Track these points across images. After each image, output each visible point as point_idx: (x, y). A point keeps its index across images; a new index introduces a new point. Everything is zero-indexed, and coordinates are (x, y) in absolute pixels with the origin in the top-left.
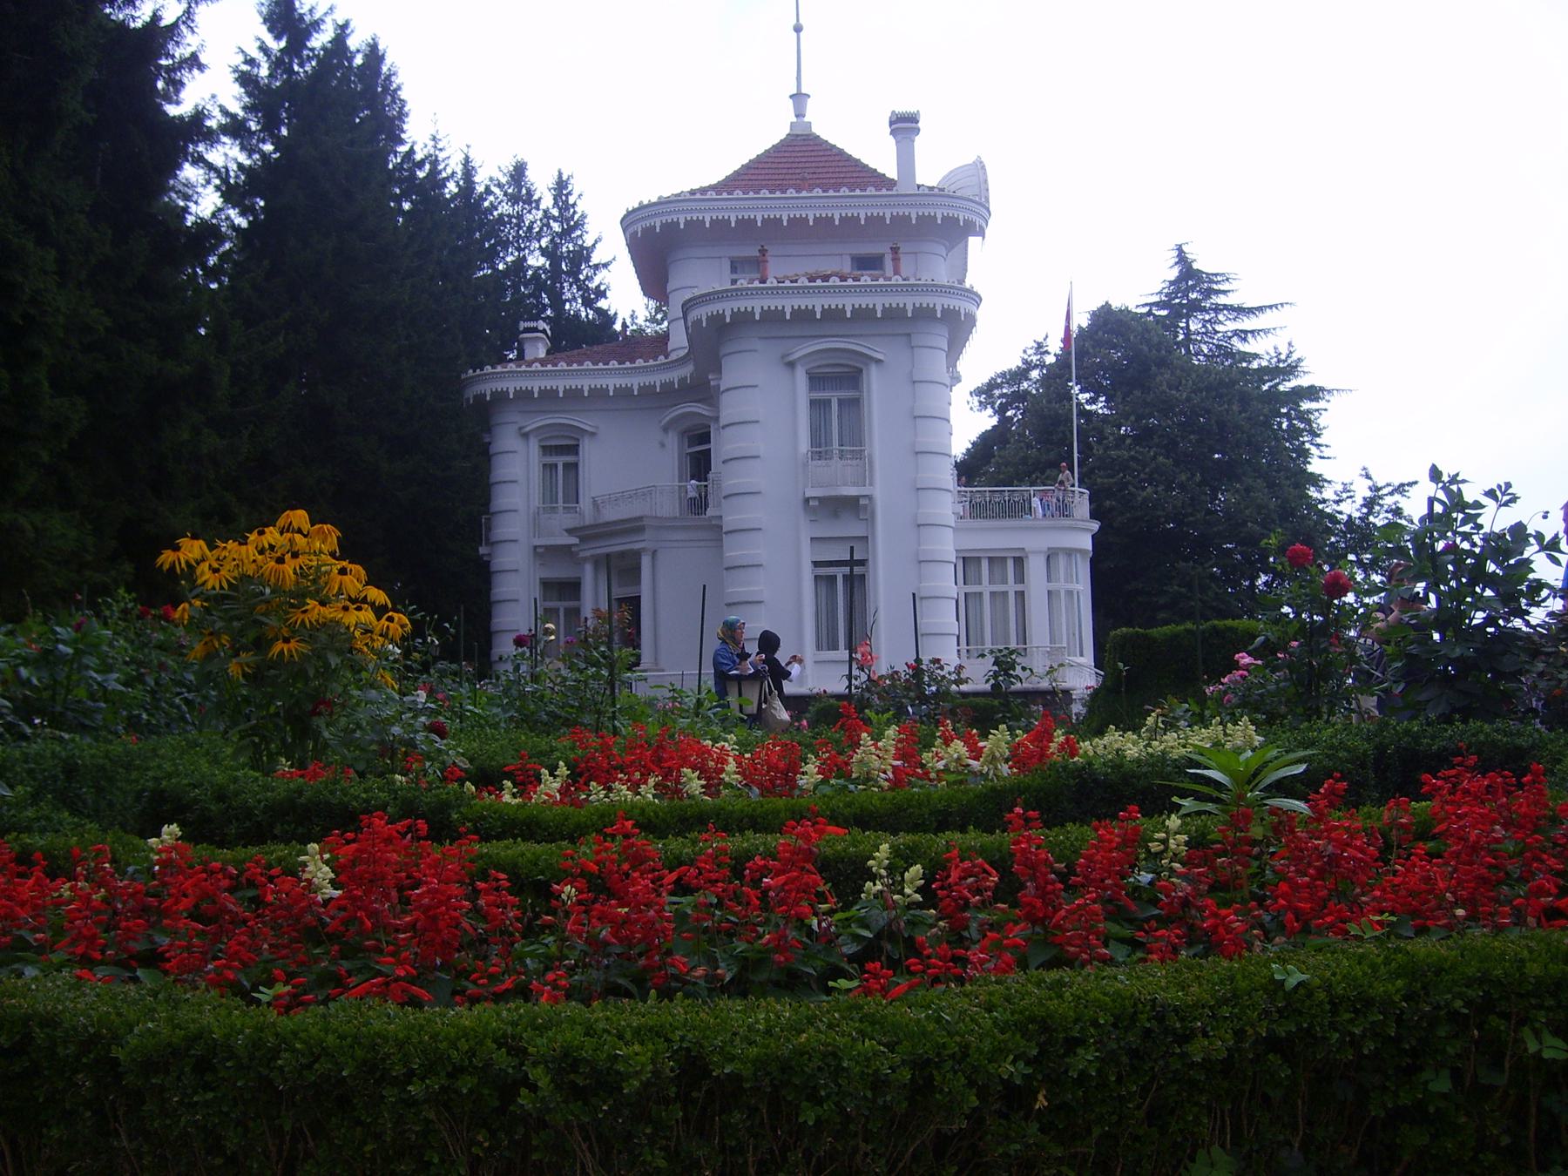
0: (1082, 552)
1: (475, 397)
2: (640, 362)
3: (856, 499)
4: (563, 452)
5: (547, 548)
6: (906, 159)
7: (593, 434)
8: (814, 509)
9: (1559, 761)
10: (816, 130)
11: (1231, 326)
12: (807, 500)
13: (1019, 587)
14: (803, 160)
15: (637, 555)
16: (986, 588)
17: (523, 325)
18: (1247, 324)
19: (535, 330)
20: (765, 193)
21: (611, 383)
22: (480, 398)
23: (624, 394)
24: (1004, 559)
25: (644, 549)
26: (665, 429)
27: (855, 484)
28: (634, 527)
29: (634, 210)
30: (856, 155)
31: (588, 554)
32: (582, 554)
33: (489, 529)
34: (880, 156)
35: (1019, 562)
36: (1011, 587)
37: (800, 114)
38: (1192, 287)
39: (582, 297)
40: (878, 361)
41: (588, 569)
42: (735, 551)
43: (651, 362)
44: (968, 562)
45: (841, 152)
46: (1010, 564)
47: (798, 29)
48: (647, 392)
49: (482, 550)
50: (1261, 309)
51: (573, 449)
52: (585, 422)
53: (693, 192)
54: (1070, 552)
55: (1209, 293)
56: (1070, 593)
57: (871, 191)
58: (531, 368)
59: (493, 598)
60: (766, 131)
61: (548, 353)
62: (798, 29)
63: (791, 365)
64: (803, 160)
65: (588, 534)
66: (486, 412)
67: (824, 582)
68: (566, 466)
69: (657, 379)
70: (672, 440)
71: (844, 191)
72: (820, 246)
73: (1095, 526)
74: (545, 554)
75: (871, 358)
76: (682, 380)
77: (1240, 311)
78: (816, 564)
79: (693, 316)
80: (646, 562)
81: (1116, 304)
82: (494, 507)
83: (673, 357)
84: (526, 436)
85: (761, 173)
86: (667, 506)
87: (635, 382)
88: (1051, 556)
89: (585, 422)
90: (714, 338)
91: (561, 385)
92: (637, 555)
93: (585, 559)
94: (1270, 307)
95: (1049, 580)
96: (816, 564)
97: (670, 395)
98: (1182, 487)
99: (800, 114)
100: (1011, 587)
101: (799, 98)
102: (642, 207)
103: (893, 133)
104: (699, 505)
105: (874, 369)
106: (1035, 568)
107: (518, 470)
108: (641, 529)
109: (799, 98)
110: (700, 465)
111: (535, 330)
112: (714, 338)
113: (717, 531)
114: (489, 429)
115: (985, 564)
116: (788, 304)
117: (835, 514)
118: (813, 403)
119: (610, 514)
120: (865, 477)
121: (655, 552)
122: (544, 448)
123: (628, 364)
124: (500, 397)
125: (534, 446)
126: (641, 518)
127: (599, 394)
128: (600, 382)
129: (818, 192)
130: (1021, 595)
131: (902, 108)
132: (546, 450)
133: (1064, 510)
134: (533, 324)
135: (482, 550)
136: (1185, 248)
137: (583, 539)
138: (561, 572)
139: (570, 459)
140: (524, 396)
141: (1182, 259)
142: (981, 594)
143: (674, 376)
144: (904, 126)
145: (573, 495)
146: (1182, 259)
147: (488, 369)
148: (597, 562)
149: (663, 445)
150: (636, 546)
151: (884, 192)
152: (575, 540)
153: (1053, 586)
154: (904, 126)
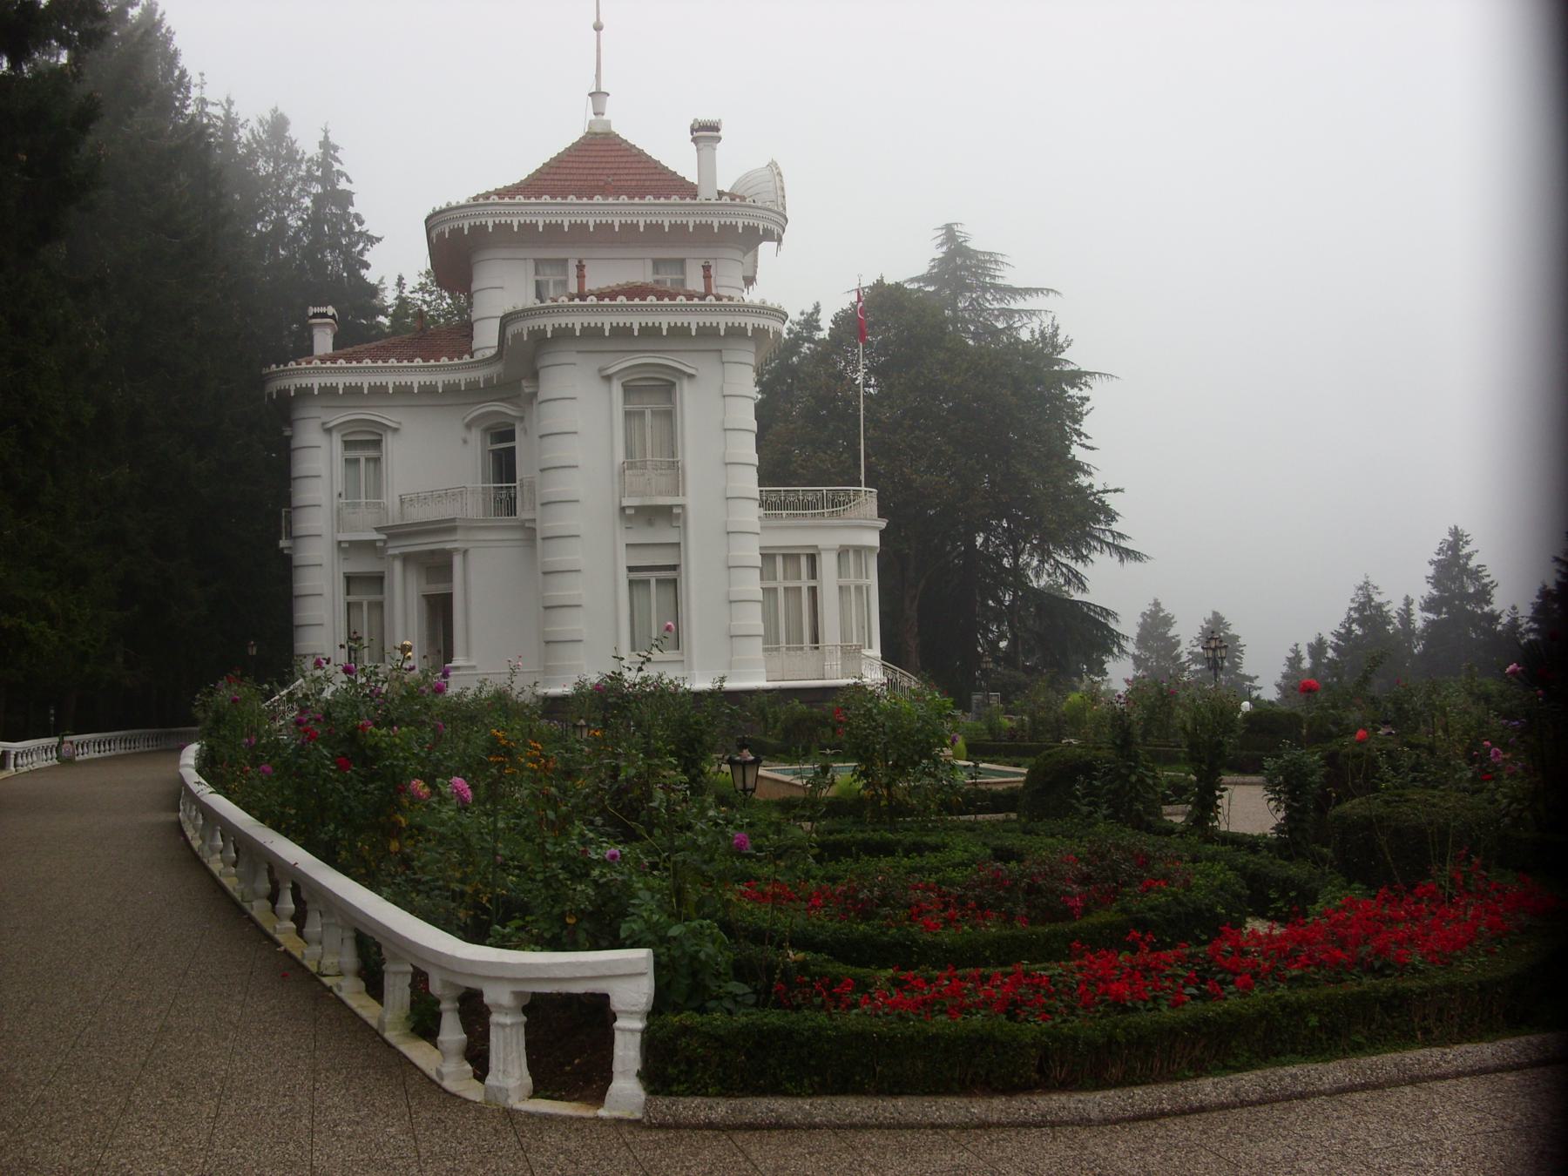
0: (870, 548)
1: (279, 392)
2: (444, 360)
3: (671, 507)
4: (365, 444)
5: (350, 542)
6: (706, 166)
7: (396, 430)
10: (615, 129)
12: (623, 509)
13: (812, 583)
15: (448, 555)
16: (780, 584)
17: (312, 311)
19: (324, 315)
20: (572, 199)
21: (416, 380)
22: (283, 394)
23: (428, 391)
24: (798, 556)
25: (456, 549)
26: (468, 426)
27: (668, 493)
28: (446, 527)
29: (442, 212)
31: (396, 552)
32: (391, 552)
33: (290, 523)
34: (680, 159)
35: (812, 559)
36: (805, 583)
38: (961, 266)
39: (344, 261)
40: (691, 376)
41: (398, 566)
42: (560, 556)
43: (456, 361)
44: (768, 556)
45: (641, 153)
46: (804, 561)
47: (598, 28)
48: (452, 390)
49: (283, 543)
51: (377, 444)
52: (388, 416)
53: (500, 193)
54: (859, 550)
56: (859, 588)
57: (675, 199)
59: (296, 593)
61: (337, 345)
62: (598, 28)
64: (600, 163)
65: (395, 533)
66: (285, 409)
69: (462, 377)
70: (475, 437)
71: (649, 199)
73: (883, 524)
75: (685, 373)
76: (488, 380)
78: (631, 569)
80: (457, 561)
81: (889, 281)
82: (296, 502)
83: (478, 356)
84: (329, 431)
86: (473, 508)
87: (440, 379)
88: (843, 552)
89: (388, 416)
91: (340, 381)
92: (448, 555)
93: (394, 556)
95: (840, 576)
96: (631, 569)
97: (474, 392)
100: (805, 583)
101: (598, 95)
102: (450, 209)
103: (694, 140)
104: (508, 505)
105: (685, 383)
106: (828, 564)
107: (319, 462)
109: (598, 95)
110: (504, 466)
113: (529, 534)
114: (289, 422)
115: (779, 560)
117: (650, 523)
119: (419, 514)
120: (677, 487)
121: (465, 552)
122: (346, 442)
123: (405, 363)
124: (305, 393)
125: (337, 440)
126: (453, 520)
127: (403, 391)
128: (405, 379)
129: (624, 199)
130: (813, 591)
131: (706, 116)
132: (348, 445)
134: (323, 310)
135: (283, 543)
139: (372, 453)
140: (329, 392)
142: (799, 589)
143: (480, 375)
144: (705, 133)
145: (377, 490)
147: (292, 365)
148: (406, 558)
149: (465, 442)
150: (448, 546)
151: (688, 200)
153: (844, 582)
154: (705, 133)
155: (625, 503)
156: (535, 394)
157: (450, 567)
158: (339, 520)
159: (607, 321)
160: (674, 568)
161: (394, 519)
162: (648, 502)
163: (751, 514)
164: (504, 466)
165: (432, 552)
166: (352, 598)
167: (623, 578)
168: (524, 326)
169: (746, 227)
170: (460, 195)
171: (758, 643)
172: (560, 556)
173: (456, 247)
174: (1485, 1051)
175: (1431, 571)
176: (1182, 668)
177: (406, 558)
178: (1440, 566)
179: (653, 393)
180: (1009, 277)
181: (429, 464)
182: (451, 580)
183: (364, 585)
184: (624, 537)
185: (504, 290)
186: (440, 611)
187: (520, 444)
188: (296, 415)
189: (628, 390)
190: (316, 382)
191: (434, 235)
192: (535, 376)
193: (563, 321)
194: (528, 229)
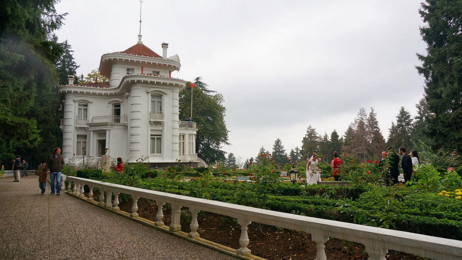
0: (195, 135)
6: (165, 53)
8: (152, 124)
10: (143, 43)
12: (150, 122)
14: (140, 49)
15: (105, 131)
17: (69, 76)
19: (72, 77)
23: (100, 95)
26: (109, 103)
28: (106, 124)
30: (153, 50)
33: (63, 122)
34: (159, 51)
36: (182, 141)
41: (92, 133)
47: (140, 22)
48: (106, 95)
49: (61, 127)
50: (211, 91)
51: (86, 106)
53: (121, 52)
58: (71, 87)
60: (133, 42)
62: (140, 22)
63: (148, 93)
64: (140, 49)
65: (92, 125)
67: (153, 139)
68: (84, 109)
69: (109, 92)
70: (111, 106)
72: (139, 68)
73: (197, 130)
74: (78, 129)
76: (115, 93)
78: (151, 135)
79: (125, 81)
80: (107, 132)
82: (65, 117)
83: (113, 88)
84: (75, 102)
85: (130, 51)
86: (109, 120)
88: (190, 135)
90: (127, 87)
92: (105, 131)
93: (91, 131)
96: (151, 135)
97: (111, 95)
100: (182, 141)
101: (140, 36)
102: (108, 54)
105: (165, 95)
107: (72, 109)
108: (107, 125)
109: (140, 36)
110: (117, 112)
111: (72, 77)
112: (127, 87)
113: (125, 127)
116: (162, 81)
118: (152, 101)
119: (96, 121)
120: (162, 118)
124: (70, 92)
125: (77, 104)
127: (94, 94)
128: (94, 91)
130: (183, 143)
132: (79, 105)
133: (191, 126)
134: (71, 76)
137: (90, 126)
138: (82, 133)
139: (85, 108)
140: (76, 93)
143: (113, 92)
144: (165, 45)
145: (86, 116)
148: (94, 131)
150: (105, 129)
152: (87, 126)
154: (165, 45)
155: (151, 120)
156: (129, 96)
157: (106, 134)
158: (76, 122)
159: (149, 80)
160: (160, 135)
161: (90, 122)
162: (156, 120)
163: (177, 125)
164: (117, 112)
165: (101, 130)
166: (78, 140)
167: (150, 137)
168: (130, 79)
169: (173, 66)
170: (111, 50)
171: (178, 153)
172: (134, 131)
173: (108, 65)
174: (175, 217)
175: (273, 147)
176: (288, 158)
177: (94, 131)
178: (275, 146)
179: (158, 97)
180: (208, 88)
181: (100, 111)
182: (106, 137)
183: (82, 138)
184: (150, 128)
185: (118, 76)
186: (102, 145)
187: (122, 108)
188: (66, 97)
189: (152, 96)
190: (73, 90)
191: (104, 60)
192: (129, 91)
193: (139, 79)
194: (127, 60)
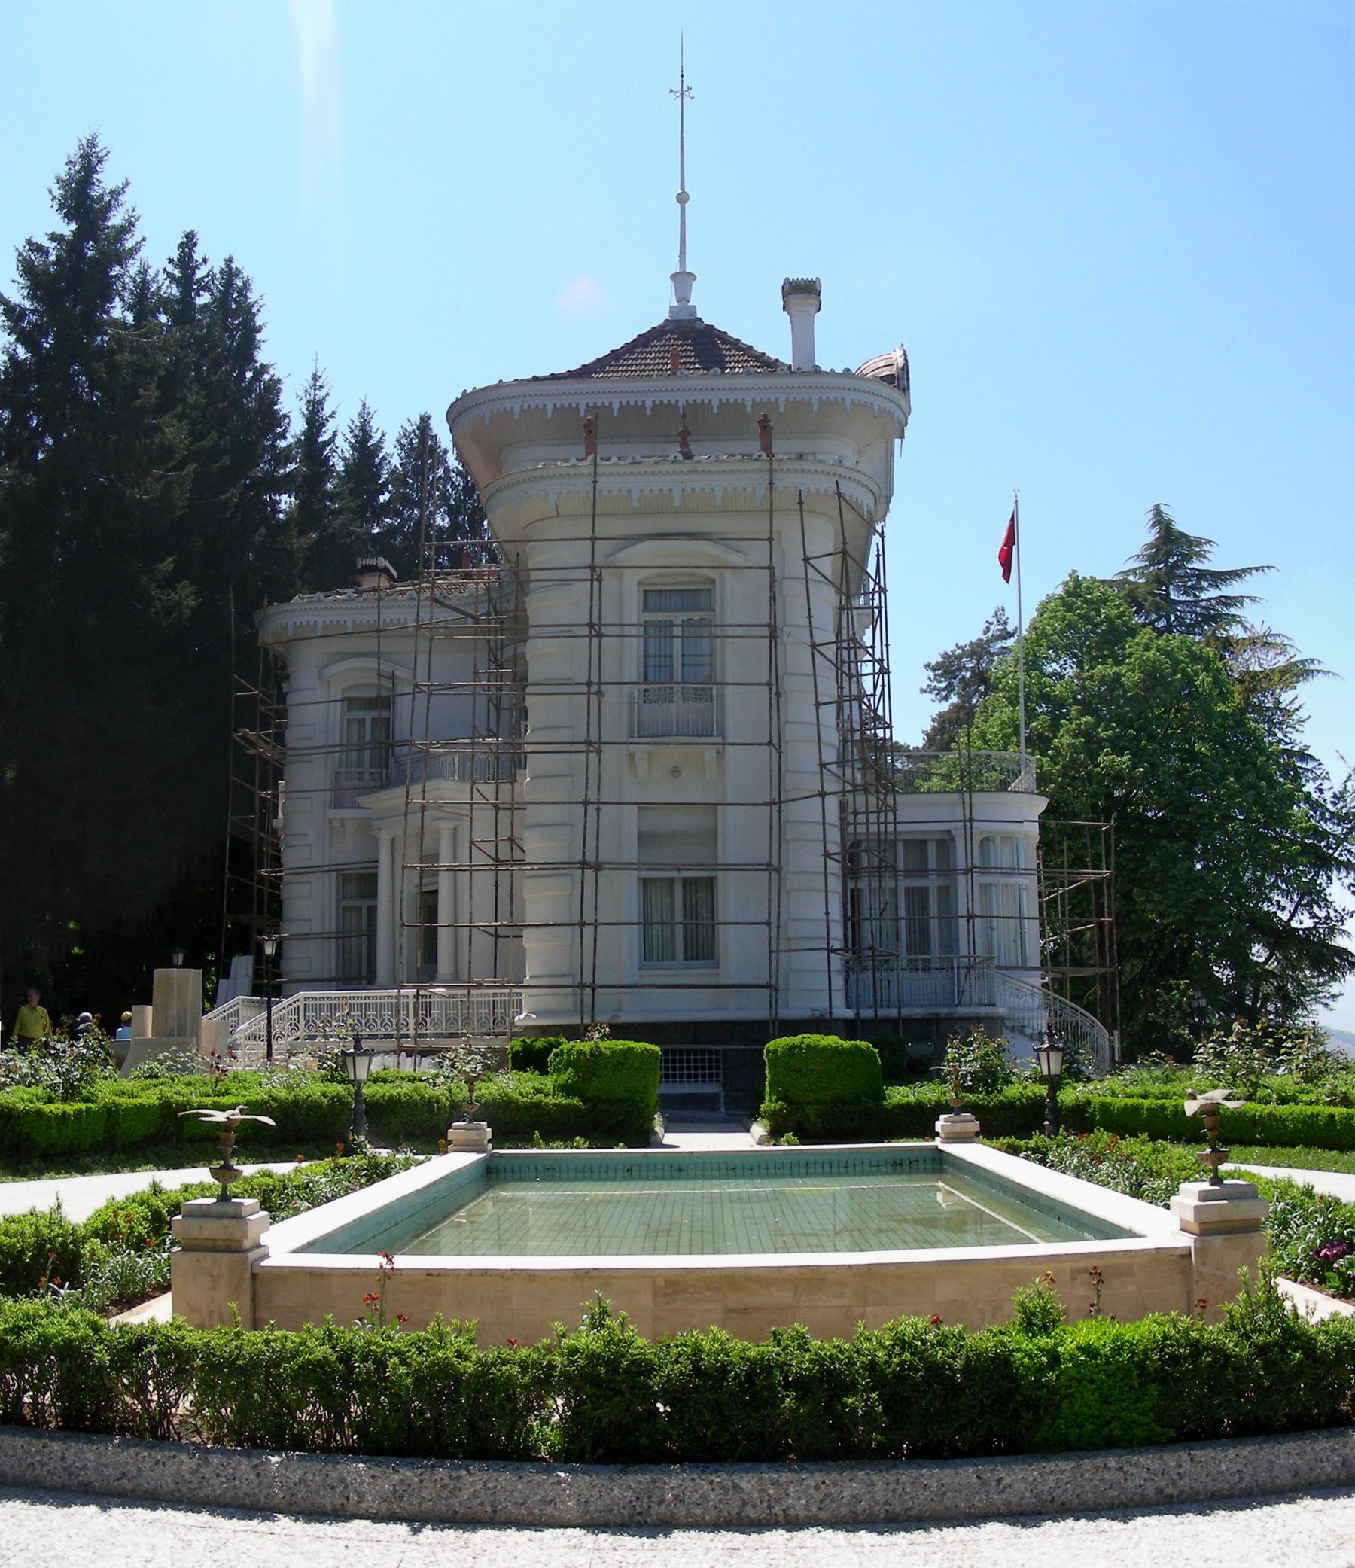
6: (803, 338)
9: (94, 146)
11: (1213, 593)
18: (1229, 590)
34: (767, 332)
37: (683, 297)
47: (682, 198)
55: (1187, 558)
60: (656, 316)
62: (682, 198)
77: (1218, 578)
94: (1257, 569)
98: (1271, 1013)
99: (683, 297)
101: (683, 280)
109: (683, 280)
136: (1163, 508)
141: (1160, 520)
144: (801, 294)
146: (1160, 520)
154: (801, 294)
